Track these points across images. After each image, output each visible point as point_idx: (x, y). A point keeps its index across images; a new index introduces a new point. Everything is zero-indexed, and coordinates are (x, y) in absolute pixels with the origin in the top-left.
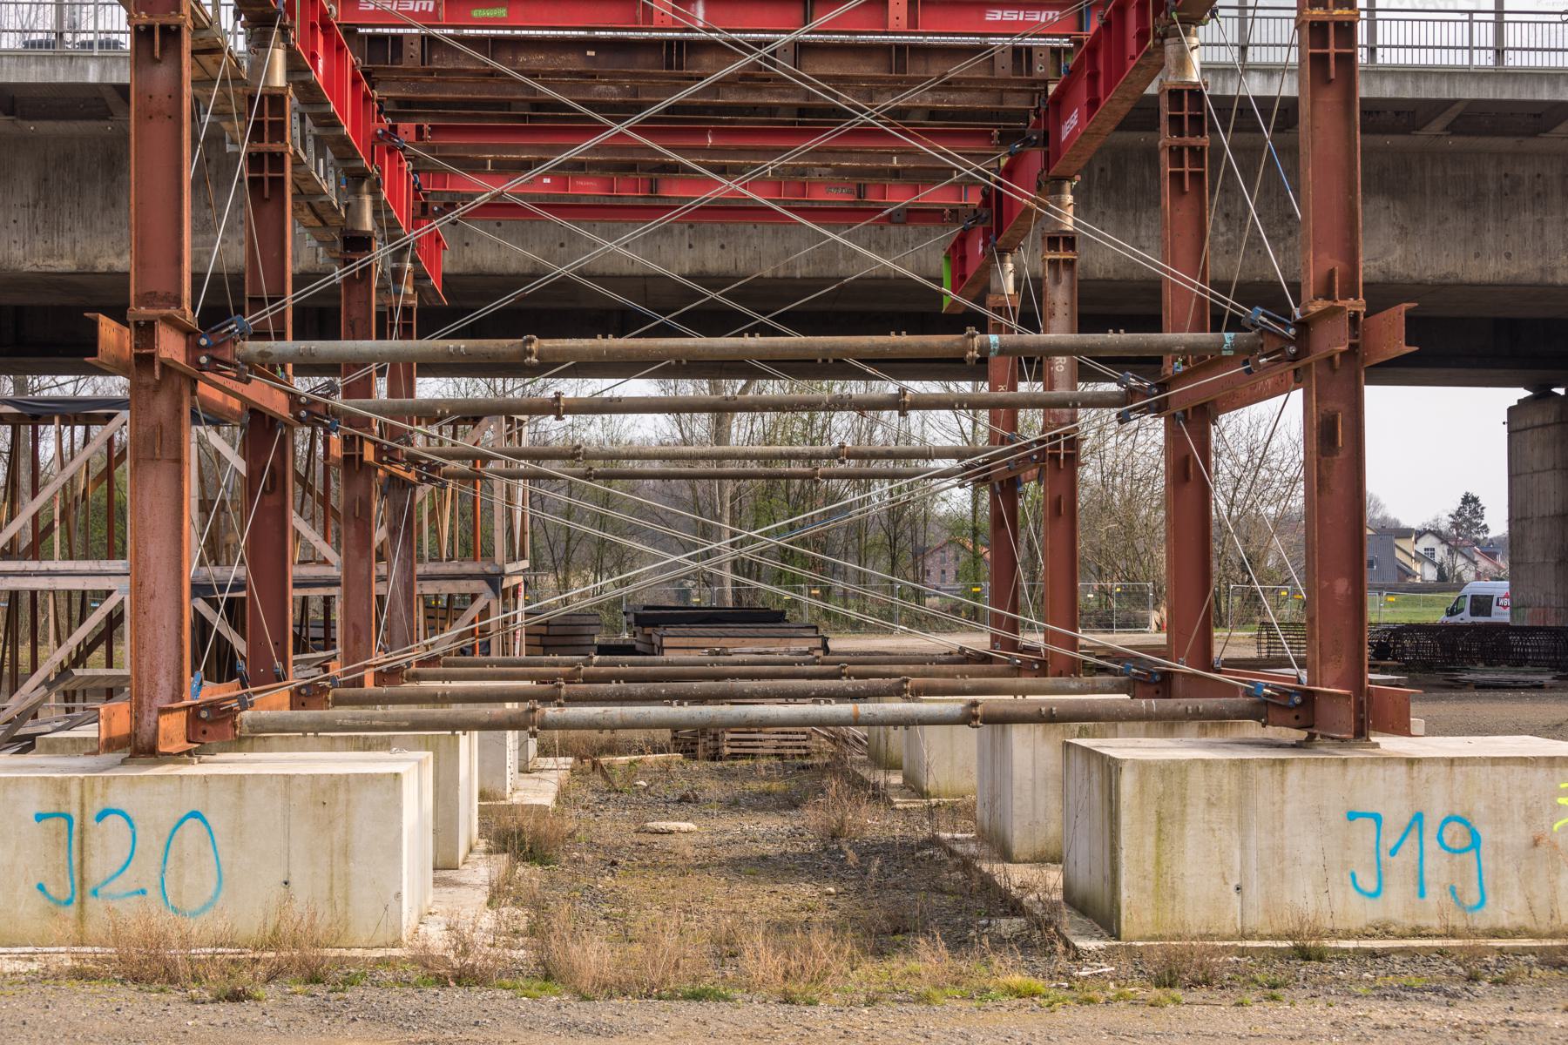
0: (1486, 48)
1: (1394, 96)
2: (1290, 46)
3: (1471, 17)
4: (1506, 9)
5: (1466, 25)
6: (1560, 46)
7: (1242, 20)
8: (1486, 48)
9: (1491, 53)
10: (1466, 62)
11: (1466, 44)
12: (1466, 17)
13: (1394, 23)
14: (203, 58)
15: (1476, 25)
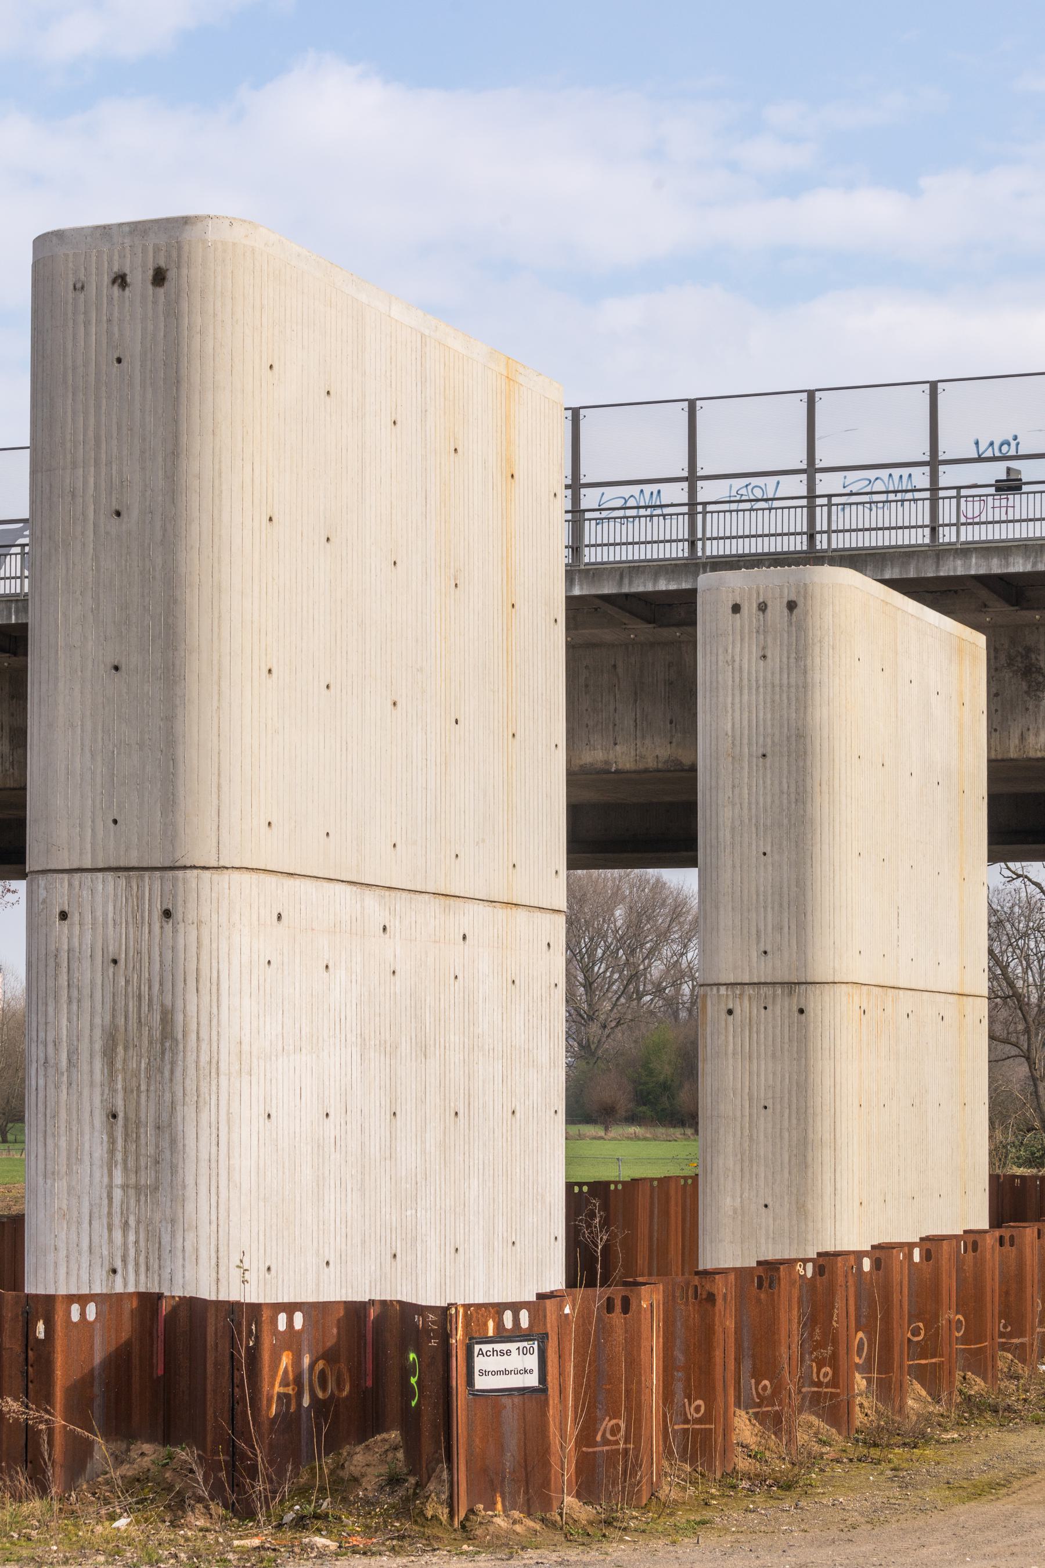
0: (677, 541)
1: (963, 573)
2: (21, 578)
3: (829, 501)
4: (818, 493)
5: (954, 501)
6: (1038, 516)
7: (692, 515)
8: (677, 541)
9: (927, 531)
10: (954, 539)
11: (954, 521)
12: (953, 493)
13: (786, 511)
14: (618, 573)
15: (834, 508)
